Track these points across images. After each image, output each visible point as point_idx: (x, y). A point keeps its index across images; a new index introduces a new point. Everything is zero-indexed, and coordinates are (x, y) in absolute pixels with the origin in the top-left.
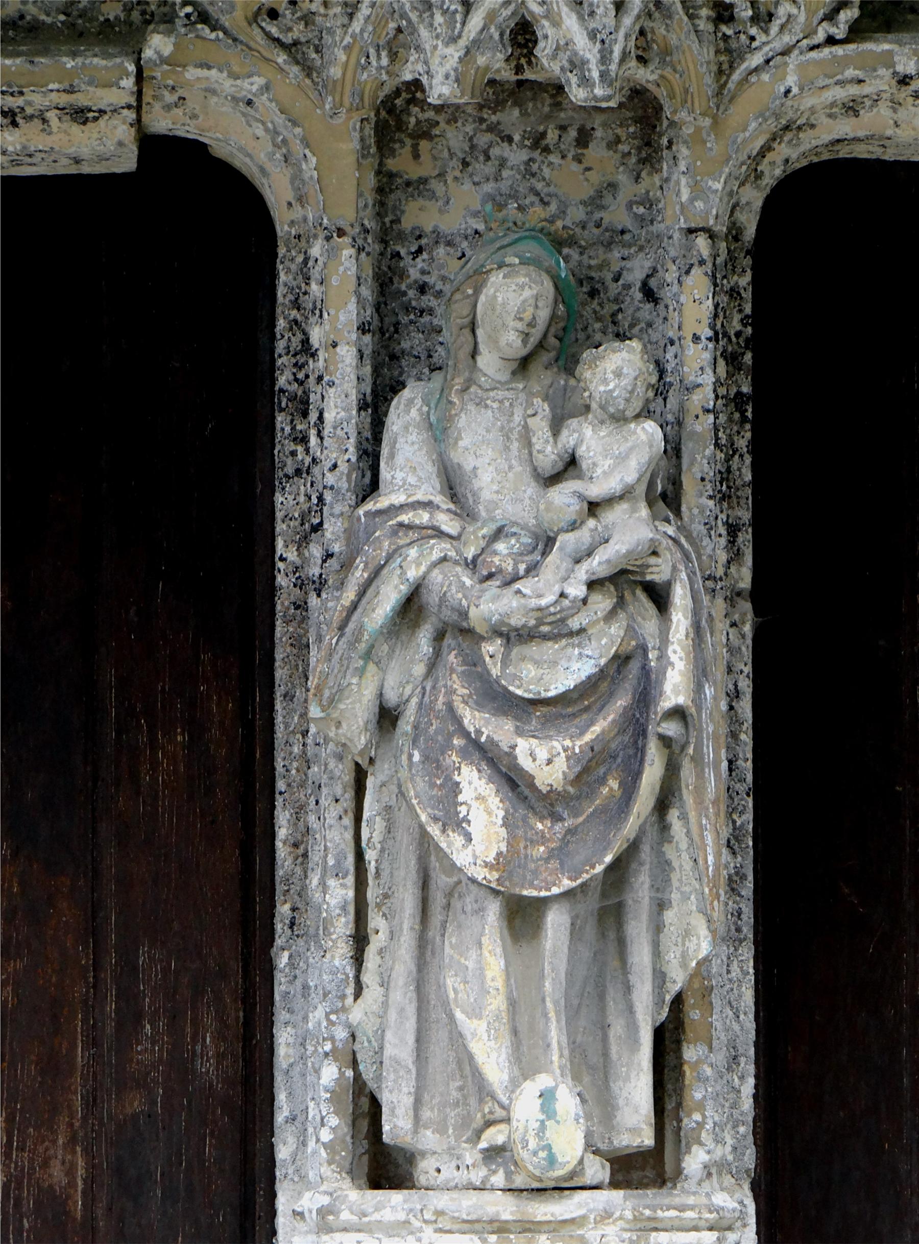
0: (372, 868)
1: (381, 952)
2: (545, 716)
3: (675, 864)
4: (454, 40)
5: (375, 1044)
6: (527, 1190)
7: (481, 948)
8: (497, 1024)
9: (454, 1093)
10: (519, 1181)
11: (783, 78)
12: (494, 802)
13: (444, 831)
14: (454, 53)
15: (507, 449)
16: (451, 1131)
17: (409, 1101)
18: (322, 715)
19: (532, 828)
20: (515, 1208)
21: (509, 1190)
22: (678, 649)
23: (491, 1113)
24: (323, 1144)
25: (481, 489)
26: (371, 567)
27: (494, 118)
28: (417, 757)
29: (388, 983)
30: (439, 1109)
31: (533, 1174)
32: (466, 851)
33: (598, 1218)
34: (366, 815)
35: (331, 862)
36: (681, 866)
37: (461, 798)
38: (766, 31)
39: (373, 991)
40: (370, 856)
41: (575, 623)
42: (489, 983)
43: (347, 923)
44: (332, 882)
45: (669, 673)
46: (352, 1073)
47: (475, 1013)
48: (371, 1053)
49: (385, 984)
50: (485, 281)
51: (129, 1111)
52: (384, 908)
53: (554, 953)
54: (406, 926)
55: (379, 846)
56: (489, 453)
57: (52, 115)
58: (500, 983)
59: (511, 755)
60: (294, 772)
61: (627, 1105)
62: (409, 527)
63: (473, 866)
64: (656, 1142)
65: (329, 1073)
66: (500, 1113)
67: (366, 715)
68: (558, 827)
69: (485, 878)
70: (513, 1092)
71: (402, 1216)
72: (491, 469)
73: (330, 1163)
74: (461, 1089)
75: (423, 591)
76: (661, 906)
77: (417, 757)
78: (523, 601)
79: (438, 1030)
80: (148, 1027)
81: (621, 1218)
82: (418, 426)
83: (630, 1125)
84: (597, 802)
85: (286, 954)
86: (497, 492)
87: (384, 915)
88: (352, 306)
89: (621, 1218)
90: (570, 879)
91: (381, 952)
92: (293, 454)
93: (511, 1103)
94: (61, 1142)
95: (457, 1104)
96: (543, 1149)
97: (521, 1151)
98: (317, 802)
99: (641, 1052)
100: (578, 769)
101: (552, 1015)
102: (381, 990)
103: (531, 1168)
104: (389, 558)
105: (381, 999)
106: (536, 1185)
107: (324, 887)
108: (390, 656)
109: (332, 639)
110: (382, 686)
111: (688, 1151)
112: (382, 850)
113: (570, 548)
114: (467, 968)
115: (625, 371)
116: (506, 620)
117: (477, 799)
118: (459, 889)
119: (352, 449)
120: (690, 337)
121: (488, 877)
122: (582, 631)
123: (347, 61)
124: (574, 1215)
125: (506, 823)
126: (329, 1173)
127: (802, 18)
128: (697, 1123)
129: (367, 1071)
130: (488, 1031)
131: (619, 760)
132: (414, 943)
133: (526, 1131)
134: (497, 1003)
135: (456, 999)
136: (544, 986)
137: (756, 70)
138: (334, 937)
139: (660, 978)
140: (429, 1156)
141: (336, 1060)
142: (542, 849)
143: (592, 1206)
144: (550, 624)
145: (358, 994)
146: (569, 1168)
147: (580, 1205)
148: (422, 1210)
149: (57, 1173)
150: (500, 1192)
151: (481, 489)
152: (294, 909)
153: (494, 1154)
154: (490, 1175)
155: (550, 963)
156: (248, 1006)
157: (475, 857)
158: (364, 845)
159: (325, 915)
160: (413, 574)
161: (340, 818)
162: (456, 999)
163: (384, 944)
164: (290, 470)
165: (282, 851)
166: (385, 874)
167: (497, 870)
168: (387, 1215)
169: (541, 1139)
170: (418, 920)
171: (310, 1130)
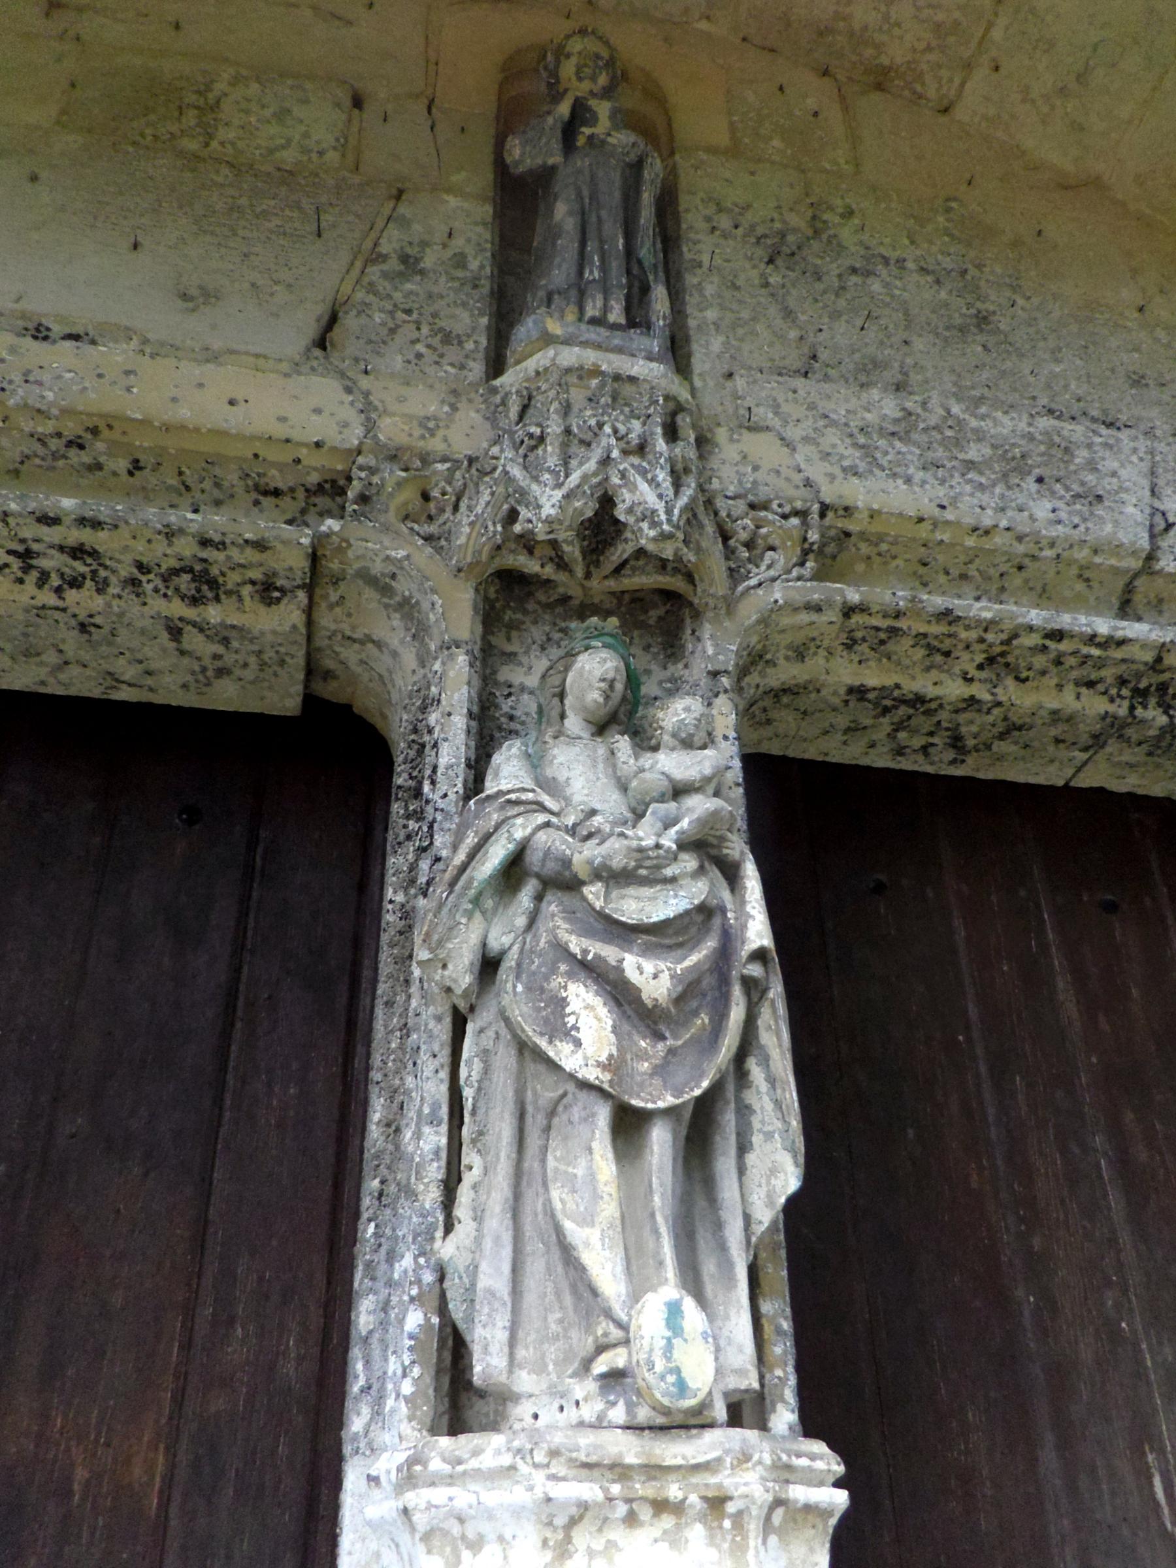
0: (468, 1105)
1: (475, 1187)
2: (645, 944)
3: (756, 1107)
4: (559, 486)
5: (466, 1280)
6: (650, 1428)
7: (591, 1153)
8: (611, 1232)
9: (553, 1326)
10: (643, 1414)
11: (773, 592)
12: (603, 1011)
13: (550, 1042)
14: (558, 494)
15: (595, 767)
16: (551, 1367)
17: (502, 1336)
18: (430, 956)
19: (636, 1044)
20: (639, 1449)
21: (628, 1428)
22: (756, 905)
23: (606, 1335)
24: (405, 1397)
25: (572, 794)
26: (480, 835)
27: (563, 625)
28: (520, 988)
29: (481, 1218)
30: (535, 1348)
31: (662, 1404)
32: (576, 1056)
33: (735, 1462)
34: (465, 1055)
35: (426, 1110)
36: (762, 1108)
37: (568, 1010)
38: (758, 566)
39: (465, 1228)
40: (468, 1093)
41: (669, 872)
42: (601, 1186)
43: (439, 1168)
44: (427, 1130)
45: (751, 924)
46: (438, 1320)
47: (587, 1220)
48: (462, 1291)
49: (478, 1217)
50: (573, 662)
51: (213, 1409)
52: (479, 1145)
53: (660, 1169)
54: (503, 1155)
55: (476, 1085)
56: (579, 769)
57: (246, 590)
58: (612, 1189)
59: (619, 970)
60: (390, 1064)
61: (729, 1344)
62: (517, 803)
63: (585, 1069)
64: (729, 1416)
65: (414, 1319)
66: (616, 1333)
67: (471, 957)
68: (660, 1046)
69: (597, 1078)
70: (631, 1308)
71: (506, 1460)
72: (582, 779)
73: (410, 1419)
74: (561, 1321)
75: (528, 852)
76: (743, 1148)
77: (520, 988)
78: (626, 842)
79: (533, 1262)
80: (240, 1330)
81: (760, 1462)
82: (518, 757)
83: (736, 1366)
84: (693, 1030)
85: (373, 1225)
86: (587, 795)
87: (479, 1151)
88: (465, 690)
89: (760, 1462)
90: (674, 1096)
91: (475, 1187)
92: (405, 826)
93: (630, 1320)
94: (146, 1439)
95: (556, 1338)
96: (671, 1371)
97: (647, 1375)
98: (415, 1064)
99: (739, 1289)
100: (680, 989)
101: (663, 1230)
102: (474, 1225)
103: (658, 1396)
104: (497, 827)
105: (474, 1233)
106: (660, 1420)
107: (418, 1135)
108: (495, 910)
109: (442, 892)
110: (486, 937)
111: (774, 1410)
112: (479, 1089)
113: (662, 813)
114: (575, 1176)
115: (693, 708)
116: (608, 863)
117: (586, 1008)
118: (565, 1101)
119: (460, 785)
120: (721, 736)
121: (601, 1076)
122: (673, 880)
123: (470, 533)
124: (709, 1457)
125: (615, 1030)
126: (409, 1431)
127: (782, 561)
128: (779, 1378)
129: (457, 1311)
130: (602, 1240)
131: (709, 998)
132: (511, 1171)
133: (651, 1350)
134: (609, 1209)
135: (564, 1210)
136: (652, 1201)
137: (753, 587)
138: (426, 1181)
139: (747, 1219)
140: (523, 1400)
141: (422, 1305)
142: (646, 1065)
143: (727, 1446)
144: (647, 868)
145: (449, 1228)
146: (701, 1395)
147: (713, 1447)
148: (532, 1450)
149: (137, 1471)
150: (619, 1431)
151: (572, 794)
152: (382, 1182)
153: (615, 1378)
154: (608, 1409)
155: (658, 1178)
156: (328, 1316)
157: (586, 1058)
158: (462, 1082)
159: (418, 1159)
160: (519, 834)
161: (437, 1071)
162: (564, 1210)
163: (477, 1179)
164: (401, 838)
165: (374, 1131)
166: (481, 1112)
167: (609, 1071)
168: (487, 1461)
169: (669, 1359)
170: (515, 1149)
171: (390, 1386)
